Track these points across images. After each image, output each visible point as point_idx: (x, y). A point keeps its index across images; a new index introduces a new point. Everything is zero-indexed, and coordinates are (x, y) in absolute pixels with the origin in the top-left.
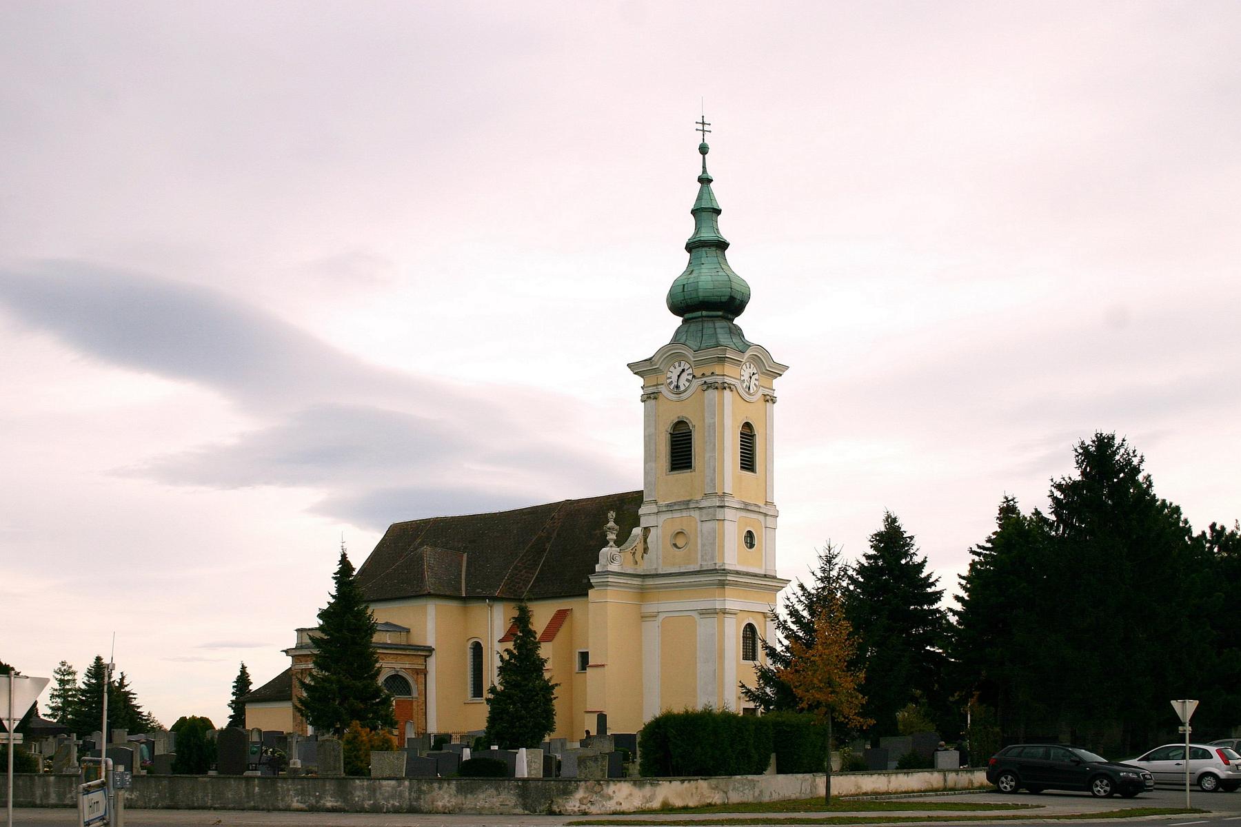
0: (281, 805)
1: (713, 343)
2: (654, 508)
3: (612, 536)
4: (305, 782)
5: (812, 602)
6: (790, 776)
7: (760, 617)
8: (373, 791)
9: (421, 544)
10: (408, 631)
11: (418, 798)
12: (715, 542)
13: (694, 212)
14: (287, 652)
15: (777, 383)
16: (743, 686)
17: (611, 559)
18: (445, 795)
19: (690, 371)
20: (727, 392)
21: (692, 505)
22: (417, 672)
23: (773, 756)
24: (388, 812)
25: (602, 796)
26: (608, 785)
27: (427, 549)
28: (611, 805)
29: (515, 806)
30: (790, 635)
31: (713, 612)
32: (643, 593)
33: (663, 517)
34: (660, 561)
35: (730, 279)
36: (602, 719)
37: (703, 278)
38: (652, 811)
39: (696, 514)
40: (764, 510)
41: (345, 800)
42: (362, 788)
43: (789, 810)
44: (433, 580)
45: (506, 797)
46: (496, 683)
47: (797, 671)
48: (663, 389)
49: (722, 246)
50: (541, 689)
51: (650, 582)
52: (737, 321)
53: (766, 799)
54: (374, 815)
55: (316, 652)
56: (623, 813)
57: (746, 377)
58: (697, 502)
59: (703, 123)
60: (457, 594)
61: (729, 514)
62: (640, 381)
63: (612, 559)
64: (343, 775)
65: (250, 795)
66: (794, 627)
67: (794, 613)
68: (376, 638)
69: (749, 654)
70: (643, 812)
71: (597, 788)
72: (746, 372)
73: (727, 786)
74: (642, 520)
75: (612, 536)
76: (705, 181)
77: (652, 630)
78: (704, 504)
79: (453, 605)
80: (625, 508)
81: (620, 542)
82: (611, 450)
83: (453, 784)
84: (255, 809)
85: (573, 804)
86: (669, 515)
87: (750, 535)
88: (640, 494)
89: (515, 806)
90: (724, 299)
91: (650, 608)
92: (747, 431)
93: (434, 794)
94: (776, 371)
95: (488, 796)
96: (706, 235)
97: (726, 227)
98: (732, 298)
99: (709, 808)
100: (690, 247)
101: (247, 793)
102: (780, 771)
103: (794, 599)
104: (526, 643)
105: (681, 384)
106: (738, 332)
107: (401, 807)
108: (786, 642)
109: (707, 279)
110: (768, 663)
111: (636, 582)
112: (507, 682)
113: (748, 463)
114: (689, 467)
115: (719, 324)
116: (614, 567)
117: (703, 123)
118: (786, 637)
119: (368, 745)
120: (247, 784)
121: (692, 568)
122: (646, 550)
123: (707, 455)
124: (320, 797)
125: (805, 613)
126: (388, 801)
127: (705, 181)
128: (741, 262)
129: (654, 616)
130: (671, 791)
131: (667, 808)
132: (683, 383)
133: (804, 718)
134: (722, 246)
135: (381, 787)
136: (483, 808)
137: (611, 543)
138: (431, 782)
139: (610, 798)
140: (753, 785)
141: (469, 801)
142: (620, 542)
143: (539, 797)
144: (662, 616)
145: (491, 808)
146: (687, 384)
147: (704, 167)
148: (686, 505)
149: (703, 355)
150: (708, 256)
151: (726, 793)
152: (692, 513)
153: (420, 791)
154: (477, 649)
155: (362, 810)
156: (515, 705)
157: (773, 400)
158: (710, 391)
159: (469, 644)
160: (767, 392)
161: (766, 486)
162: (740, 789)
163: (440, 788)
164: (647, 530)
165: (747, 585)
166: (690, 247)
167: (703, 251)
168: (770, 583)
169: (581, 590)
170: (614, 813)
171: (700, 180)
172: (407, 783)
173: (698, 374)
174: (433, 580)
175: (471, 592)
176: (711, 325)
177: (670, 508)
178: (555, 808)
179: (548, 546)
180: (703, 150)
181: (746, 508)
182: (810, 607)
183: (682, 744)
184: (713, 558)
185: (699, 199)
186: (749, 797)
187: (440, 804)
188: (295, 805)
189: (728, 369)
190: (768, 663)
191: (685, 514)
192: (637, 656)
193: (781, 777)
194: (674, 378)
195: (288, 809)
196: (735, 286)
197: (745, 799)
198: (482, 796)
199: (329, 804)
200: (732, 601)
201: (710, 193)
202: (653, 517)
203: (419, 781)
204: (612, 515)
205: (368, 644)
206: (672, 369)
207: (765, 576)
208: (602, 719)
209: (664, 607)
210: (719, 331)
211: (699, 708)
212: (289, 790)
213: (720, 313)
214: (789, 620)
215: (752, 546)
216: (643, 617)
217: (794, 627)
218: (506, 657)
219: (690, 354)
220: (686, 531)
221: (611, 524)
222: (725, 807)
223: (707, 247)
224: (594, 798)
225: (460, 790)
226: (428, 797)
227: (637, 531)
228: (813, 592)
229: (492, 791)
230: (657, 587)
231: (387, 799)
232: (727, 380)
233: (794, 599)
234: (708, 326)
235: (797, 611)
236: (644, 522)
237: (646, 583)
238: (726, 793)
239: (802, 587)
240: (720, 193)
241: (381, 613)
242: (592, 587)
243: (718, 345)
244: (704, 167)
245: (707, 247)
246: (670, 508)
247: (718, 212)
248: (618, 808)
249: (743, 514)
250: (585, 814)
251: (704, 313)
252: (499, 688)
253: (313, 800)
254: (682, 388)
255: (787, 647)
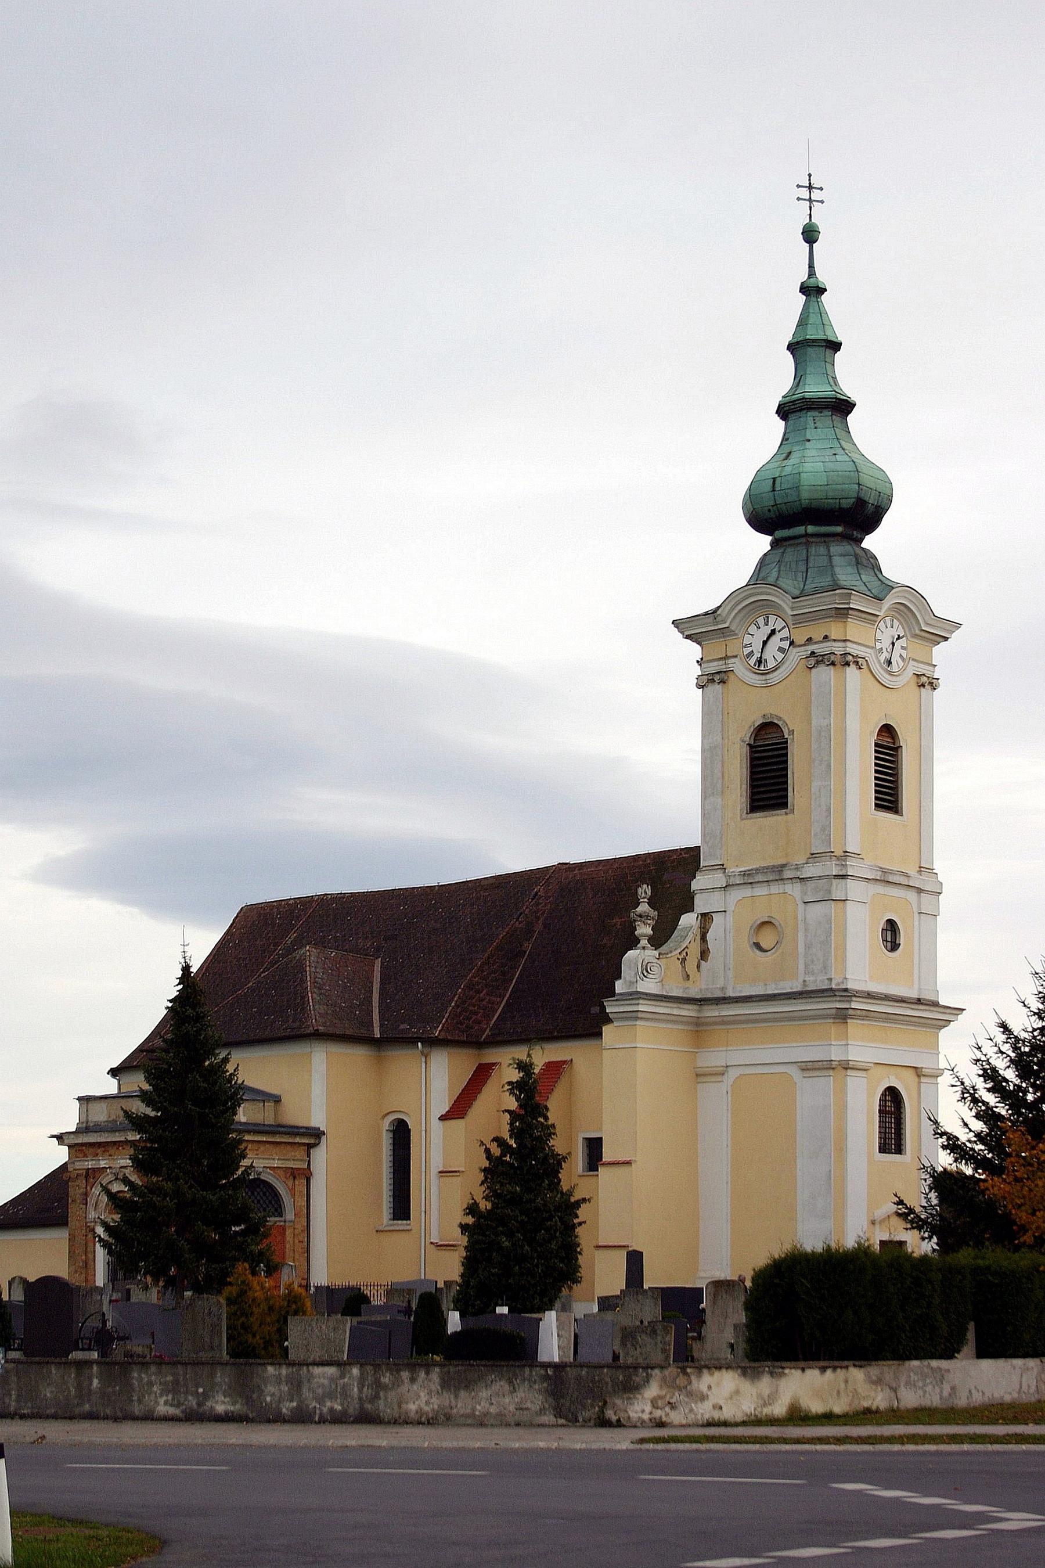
0: (137, 1409)
1: (826, 581)
2: (718, 879)
3: (644, 930)
4: (180, 1369)
5: (1021, 1055)
6: (1001, 1363)
7: (910, 1075)
8: (296, 1385)
9: (299, 943)
10: (277, 1100)
11: (377, 1397)
12: (829, 940)
13: (792, 347)
14: (60, 1138)
15: (939, 652)
16: (901, 1202)
17: (644, 970)
18: (421, 1392)
19: (785, 633)
20: (851, 670)
21: (788, 874)
22: (293, 1174)
23: (971, 1326)
24: (322, 1421)
25: (690, 1394)
26: (699, 1375)
27: (310, 953)
28: (704, 1410)
29: (542, 1411)
30: (987, 1115)
31: (827, 1066)
32: (699, 1032)
33: (736, 895)
34: (730, 974)
35: (857, 466)
36: (635, 1261)
37: (808, 467)
38: (772, 1421)
39: (794, 890)
40: (919, 884)
41: (249, 1401)
42: (279, 1380)
43: (1007, 1422)
44: (322, 1009)
45: (527, 1396)
46: (479, 1198)
47: (1017, 1180)
48: (737, 666)
49: (843, 407)
50: (558, 1208)
51: (712, 1012)
52: (869, 542)
53: (962, 1402)
54: (300, 1427)
55: (136, 1137)
56: (725, 1424)
57: (886, 644)
58: (797, 868)
59: (810, 187)
60: (364, 1032)
61: (854, 889)
62: (695, 651)
63: (646, 971)
64: (226, 1357)
65: (84, 1393)
66: (991, 1099)
67: (990, 1074)
68: (242, 1115)
69: (892, 1141)
70: (758, 1422)
71: (681, 1381)
72: (886, 632)
73: (896, 1378)
74: (698, 900)
75: (644, 930)
76: (812, 290)
77: (716, 1099)
78: (809, 871)
79: (358, 1055)
80: (668, 876)
81: (658, 941)
82: (644, 773)
83: (436, 1374)
84: (92, 1416)
85: (640, 1408)
86: (747, 892)
87: (891, 926)
88: (693, 853)
89: (542, 1411)
90: (846, 504)
91: (713, 1058)
92: (886, 741)
93: (404, 1389)
94: (936, 632)
95: (495, 1395)
96: (814, 388)
97: (849, 374)
98: (861, 502)
99: (867, 1415)
100: (785, 411)
101: (79, 1387)
102: (983, 1352)
103: (989, 1050)
104: (530, 1126)
105: (768, 655)
106: (869, 563)
107: (344, 1412)
108: (978, 1126)
109: (816, 470)
110: (945, 1160)
111: (688, 1011)
112: (496, 1195)
113: (888, 797)
114: (784, 805)
115: (836, 548)
116: (648, 986)
117: (810, 187)
118: (978, 1116)
119: (264, 1306)
120: (78, 1375)
121: (788, 987)
122: (704, 954)
123: (816, 784)
124: (206, 1396)
125: (1010, 1074)
126: (321, 1400)
127: (812, 290)
128: (875, 436)
129: (721, 1073)
130: (805, 1387)
131: (797, 1416)
132: (772, 654)
133: (1024, 1260)
134: (843, 407)
135: (311, 1377)
136: (486, 1414)
137: (644, 942)
138: (396, 1369)
139: (703, 1398)
140: (941, 1377)
141: (464, 1403)
142: (658, 941)
143: (584, 1392)
144: (733, 1074)
145: (500, 1415)
146: (780, 656)
147: (811, 266)
148: (777, 873)
149: (808, 605)
150: (818, 428)
151: (895, 1391)
152: (789, 888)
153: (378, 1385)
154: (401, 1133)
155: (278, 1419)
156: (510, 1234)
157: (933, 684)
158: (822, 668)
159: (386, 1124)
160: (922, 669)
161: (921, 838)
162: (917, 1383)
163: (413, 1380)
164: (706, 918)
165: (887, 1017)
166: (785, 411)
167: (809, 418)
168: (929, 1014)
169: (589, 1025)
170: (710, 1424)
171: (804, 289)
172: (355, 1371)
173: (800, 639)
174: (322, 1009)
175: (391, 1030)
176: (822, 550)
177: (749, 879)
178: (610, 1414)
179: (528, 946)
180: (810, 235)
181: (885, 879)
182: (1020, 1063)
183: (808, 1307)
184: (825, 968)
185: (802, 323)
186: (933, 1397)
187: (412, 1407)
188: (162, 1409)
189: (854, 629)
190: (945, 1160)
191: (775, 889)
192: (702, 1153)
193: (986, 1364)
194: (757, 647)
195: (149, 1417)
196: (866, 480)
197: (927, 1402)
198: (484, 1394)
199: (220, 1408)
200: (861, 1046)
201: (822, 313)
202: (718, 895)
203: (377, 1367)
204: (645, 891)
205: (228, 1124)
206: (753, 629)
207: (919, 1001)
208: (635, 1261)
209: (737, 1056)
210: (836, 560)
211: (850, 1243)
212: (151, 1384)
213: (839, 529)
214: (981, 1084)
215: (894, 946)
216: (700, 1076)
217: (991, 1099)
218: (496, 1151)
219: (785, 604)
220: (778, 917)
221: (644, 908)
222: (894, 1415)
223: (815, 408)
224: (676, 1397)
225: (446, 1384)
226: (392, 1395)
227: (688, 920)
228: (1024, 1035)
229: (502, 1385)
230: (724, 1021)
231: (321, 1400)
232: (852, 649)
233: (989, 1050)
234: (818, 551)
235: (994, 1070)
236: (701, 904)
237: (705, 1014)
238: (895, 1391)
239: (1004, 1027)
240: (840, 313)
241: (252, 1068)
242: (608, 1020)
243: (835, 586)
244: (811, 266)
245: (815, 408)
246: (749, 879)
247: (836, 346)
248: (716, 1415)
249: (880, 889)
250: (661, 1424)
251: (811, 529)
252: (485, 1205)
253: (192, 1402)
254: (771, 664)
255: (978, 1135)
